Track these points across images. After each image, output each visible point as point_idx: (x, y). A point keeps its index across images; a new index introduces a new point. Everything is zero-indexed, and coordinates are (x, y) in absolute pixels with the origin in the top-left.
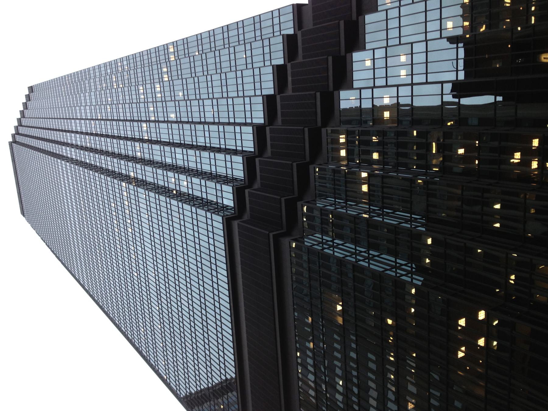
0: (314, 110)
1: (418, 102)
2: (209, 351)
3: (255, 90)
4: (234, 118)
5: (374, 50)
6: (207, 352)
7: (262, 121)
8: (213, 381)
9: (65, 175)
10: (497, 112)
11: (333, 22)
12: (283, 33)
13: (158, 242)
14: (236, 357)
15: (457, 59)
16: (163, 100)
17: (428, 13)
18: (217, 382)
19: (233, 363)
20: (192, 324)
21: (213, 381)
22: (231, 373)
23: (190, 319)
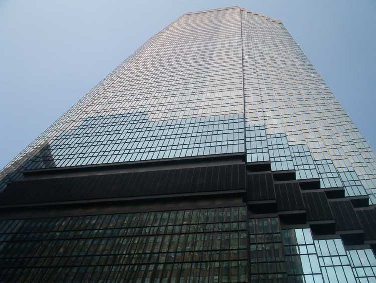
0: (268, 198)
1: (304, 260)
2: (59, 149)
3: (274, 158)
4: (251, 154)
5: (321, 274)
6: (58, 147)
7: (249, 161)
8: (56, 160)
9: (179, 48)
10: (225, 260)
11: (330, 206)
12: (321, 180)
13: (142, 118)
14: (74, 168)
15: (261, 141)
16: (268, 137)
17: (330, 258)
18: (56, 163)
19: (63, 166)
20: (85, 145)
21: (56, 160)
22: (59, 164)
23: (90, 142)
